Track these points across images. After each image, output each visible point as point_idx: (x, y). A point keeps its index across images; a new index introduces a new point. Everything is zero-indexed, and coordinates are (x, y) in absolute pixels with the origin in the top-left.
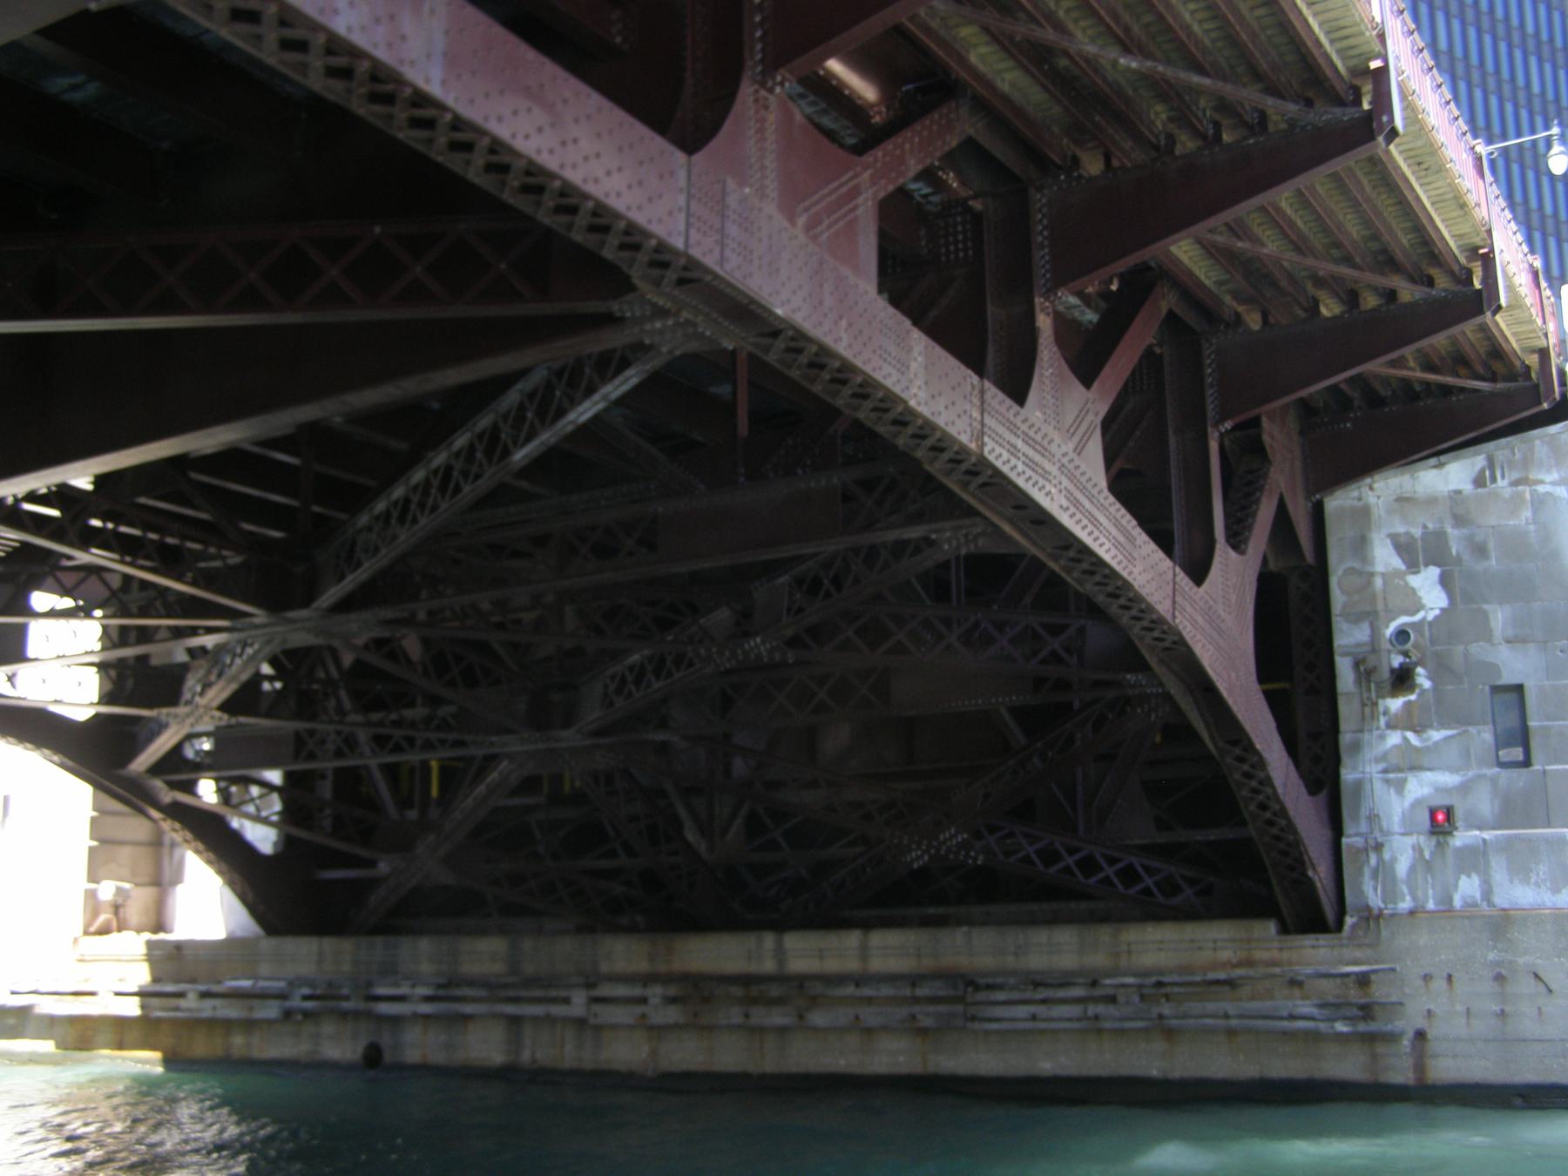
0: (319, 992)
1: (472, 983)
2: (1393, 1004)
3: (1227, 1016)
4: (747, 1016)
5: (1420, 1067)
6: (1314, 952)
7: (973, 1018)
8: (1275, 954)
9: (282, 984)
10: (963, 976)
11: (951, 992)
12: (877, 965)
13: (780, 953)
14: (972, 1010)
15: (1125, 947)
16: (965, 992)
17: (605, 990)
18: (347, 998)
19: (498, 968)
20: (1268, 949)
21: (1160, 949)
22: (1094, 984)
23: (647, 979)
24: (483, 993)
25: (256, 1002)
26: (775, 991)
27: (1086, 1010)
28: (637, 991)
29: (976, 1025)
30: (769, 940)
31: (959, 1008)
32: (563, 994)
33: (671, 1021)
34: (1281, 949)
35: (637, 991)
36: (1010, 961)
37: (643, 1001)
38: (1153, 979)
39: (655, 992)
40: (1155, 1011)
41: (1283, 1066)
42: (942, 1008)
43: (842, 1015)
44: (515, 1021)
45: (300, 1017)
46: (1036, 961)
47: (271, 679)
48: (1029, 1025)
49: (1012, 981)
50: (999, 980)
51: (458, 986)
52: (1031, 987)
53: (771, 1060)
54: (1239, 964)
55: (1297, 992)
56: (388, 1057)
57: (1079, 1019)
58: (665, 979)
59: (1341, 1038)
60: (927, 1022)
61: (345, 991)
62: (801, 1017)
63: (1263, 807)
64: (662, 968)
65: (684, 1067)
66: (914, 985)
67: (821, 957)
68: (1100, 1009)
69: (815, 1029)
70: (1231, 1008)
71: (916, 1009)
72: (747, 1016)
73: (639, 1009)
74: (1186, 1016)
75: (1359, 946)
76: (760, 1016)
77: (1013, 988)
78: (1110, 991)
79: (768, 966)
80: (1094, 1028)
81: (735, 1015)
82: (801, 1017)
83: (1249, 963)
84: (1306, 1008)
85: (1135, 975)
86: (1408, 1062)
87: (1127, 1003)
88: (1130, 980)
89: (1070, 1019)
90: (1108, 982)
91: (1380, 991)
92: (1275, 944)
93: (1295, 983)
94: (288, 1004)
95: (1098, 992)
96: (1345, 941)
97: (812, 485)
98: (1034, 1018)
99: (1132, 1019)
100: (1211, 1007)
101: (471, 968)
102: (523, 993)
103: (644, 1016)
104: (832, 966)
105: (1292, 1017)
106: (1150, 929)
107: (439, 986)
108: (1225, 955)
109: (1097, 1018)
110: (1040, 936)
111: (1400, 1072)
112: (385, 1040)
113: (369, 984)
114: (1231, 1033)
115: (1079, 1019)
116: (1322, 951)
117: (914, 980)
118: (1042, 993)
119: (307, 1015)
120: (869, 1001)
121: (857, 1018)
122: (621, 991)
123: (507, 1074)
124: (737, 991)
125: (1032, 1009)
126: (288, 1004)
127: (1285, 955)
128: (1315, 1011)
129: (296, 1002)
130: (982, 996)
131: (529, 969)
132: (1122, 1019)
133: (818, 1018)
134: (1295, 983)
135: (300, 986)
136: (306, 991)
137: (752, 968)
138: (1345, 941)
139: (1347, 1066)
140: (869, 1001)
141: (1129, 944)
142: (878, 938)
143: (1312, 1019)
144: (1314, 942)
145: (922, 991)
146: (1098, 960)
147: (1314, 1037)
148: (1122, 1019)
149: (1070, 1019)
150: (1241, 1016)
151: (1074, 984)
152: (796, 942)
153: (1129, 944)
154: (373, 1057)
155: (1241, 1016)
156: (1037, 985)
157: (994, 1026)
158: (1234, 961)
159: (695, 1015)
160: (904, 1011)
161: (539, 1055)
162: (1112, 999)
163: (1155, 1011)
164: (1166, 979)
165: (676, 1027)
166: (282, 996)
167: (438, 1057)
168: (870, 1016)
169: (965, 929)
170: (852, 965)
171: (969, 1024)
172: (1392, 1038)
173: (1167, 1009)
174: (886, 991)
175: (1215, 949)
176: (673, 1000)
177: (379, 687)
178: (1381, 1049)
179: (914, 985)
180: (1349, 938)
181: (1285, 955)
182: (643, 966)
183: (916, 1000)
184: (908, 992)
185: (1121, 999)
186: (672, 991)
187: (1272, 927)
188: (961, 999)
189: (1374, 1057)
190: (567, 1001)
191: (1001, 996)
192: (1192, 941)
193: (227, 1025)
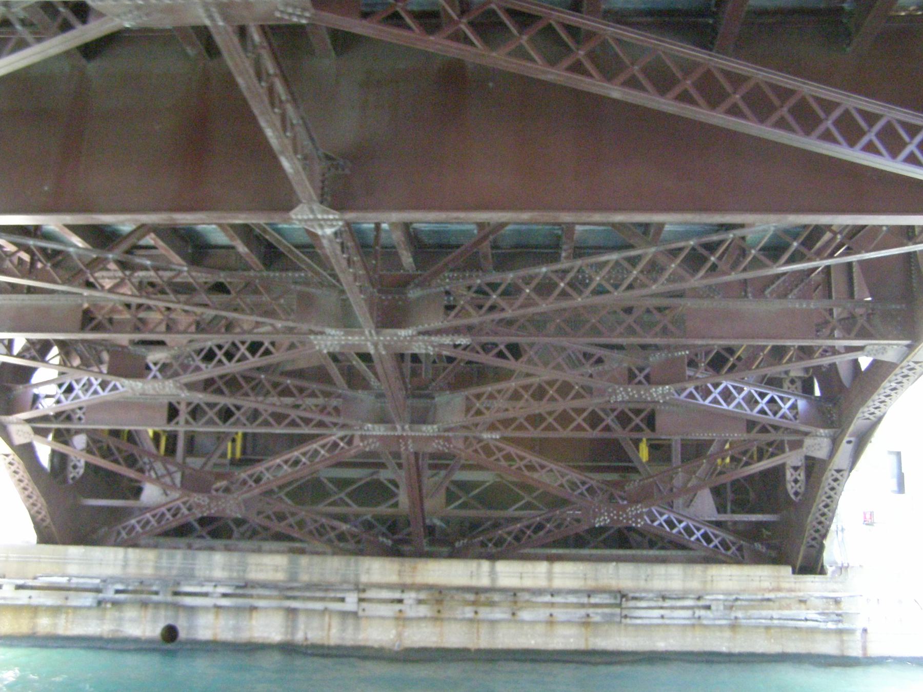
0: (130, 588)
1: (264, 585)
2: (852, 614)
3: (772, 618)
4: (476, 613)
5: (864, 648)
6: (811, 584)
7: (626, 617)
8: (793, 585)
9: (98, 581)
10: (620, 592)
11: (612, 601)
12: (558, 583)
13: (493, 574)
14: (625, 612)
15: (709, 578)
16: (621, 601)
17: (370, 594)
18: (156, 593)
19: (280, 576)
20: (789, 582)
21: (730, 580)
22: (699, 598)
23: (404, 588)
24: (275, 593)
25: (71, 594)
26: (496, 597)
27: (694, 613)
28: (397, 595)
29: (628, 621)
30: (485, 565)
31: (618, 611)
32: (339, 595)
33: (421, 614)
34: (795, 582)
35: (397, 595)
36: (642, 584)
37: (400, 601)
38: (734, 597)
39: (410, 597)
40: (733, 615)
41: (793, 646)
42: (607, 610)
43: (543, 614)
44: (292, 612)
45: (109, 605)
46: (658, 584)
47: (663, 390)
48: (660, 621)
49: (651, 595)
50: (643, 595)
51: (253, 587)
52: (661, 599)
53: (484, 641)
54: (771, 591)
55: (803, 606)
56: (183, 635)
57: (688, 619)
58: (419, 588)
59: (827, 632)
60: (597, 619)
61: (155, 588)
62: (514, 614)
63: (20, 481)
64: (408, 580)
65: (422, 644)
66: (589, 596)
67: (521, 578)
68: (703, 613)
69: (523, 622)
70: (775, 614)
71: (591, 611)
72: (476, 613)
73: (398, 607)
74: (750, 618)
75: (836, 582)
76: (485, 613)
77: (651, 599)
78: (707, 603)
79: (485, 582)
80: (696, 625)
81: (469, 612)
82: (514, 614)
83: (779, 589)
84: (812, 614)
85: (723, 594)
86: (859, 645)
87: (717, 610)
88: (721, 597)
89: (684, 618)
90: (708, 597)
91: (845, 607)
92: (792, 580)
93: (802, 601)
94: (101, 596)
95: (701, 603)
96: (829, 580)
97: (797, 306)
98: (662, 617)
99: (719, 619)
100: (764, 613)
101: (254, 575)
102: (308, 594)
103: (400, 611)
104: (528, 583)
105: (806, 620)
106: (724, 568)
107: (238, 587)
108: (766, 584)
109: (699, 618)
110: (660, 570)
111: (855, 651)
112: (182, 624)
113: (178, 584)
114: (768, 628)
115: (688, 619)
116: (817, 584)
117: (590, 593)
118: (668, 603)
119: (115, 603)
120: (596, 606)
121: (551, 615)
122: (385, 594)
123: (288, 649)
124: (471, 597)
125: (662, 612)
126: (101, 596)
127: (798, 585)
128: (818, 617)
129: (110, 594)
130: (632, 604)
131: (304, 577)
132: (715, 619)
133: (525, 615)
134: (802, 601)
135: (113, 583)
136: (120, 587)
137: (474, 583)
138: (829, 580)
139: (828, 647)
140: (596, 606)
141: (712, 576)
142: (558, 567)
143: (817, 621)
144: (813, 579)
145: (593, 600)
146: (694, 584)
147: (813, 631)
148: (715, 619)
149: (684, 618)
150: (779, 619)
151: (687, 598)
152: (502, 566)
153: (712, 576)
154: (170, 633)
155: (779, 619)
156: (664, 598)
157: (639, 621)
158: (770, 588)
159: (439, 612)
160: (582, 612)
161: (310, 636)
162: (708, 608)
163: (733, 615)
164: (741, 597)
165: (424, 618)
166: (98, 590)
167: (227, 635)
168: (560, 614)
169: (614, 564)
170: (542, 583)
171: (624, 620)
172: (850, 632)
173: (740, 614)
174: (572, 599)
175: (760, 581)
176: (420, 602)
177: (289, 381)
178: (845, 637)
179: (589, 596)
180: (831, 578)
181: (798, 585)
182: (394, 579)
183: (553, 605)
184: (585, 600)
185: (713, 607)
186: (423, 596)
187: (789, 569)
188: (619, 605)
189: (842, 641)
190: (342, 600)
191: (643, 604)
192: (748, 576)
193: (35, 610)
